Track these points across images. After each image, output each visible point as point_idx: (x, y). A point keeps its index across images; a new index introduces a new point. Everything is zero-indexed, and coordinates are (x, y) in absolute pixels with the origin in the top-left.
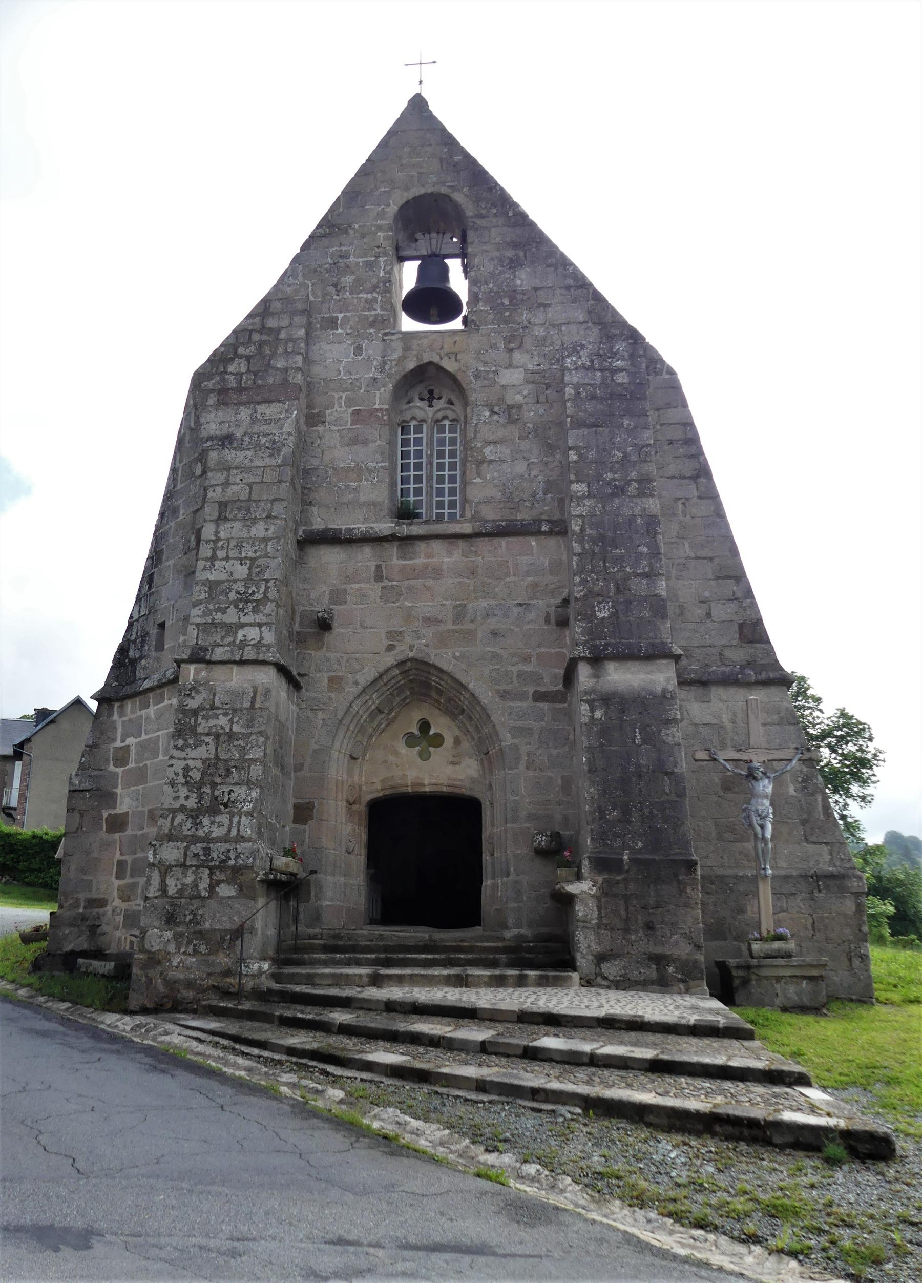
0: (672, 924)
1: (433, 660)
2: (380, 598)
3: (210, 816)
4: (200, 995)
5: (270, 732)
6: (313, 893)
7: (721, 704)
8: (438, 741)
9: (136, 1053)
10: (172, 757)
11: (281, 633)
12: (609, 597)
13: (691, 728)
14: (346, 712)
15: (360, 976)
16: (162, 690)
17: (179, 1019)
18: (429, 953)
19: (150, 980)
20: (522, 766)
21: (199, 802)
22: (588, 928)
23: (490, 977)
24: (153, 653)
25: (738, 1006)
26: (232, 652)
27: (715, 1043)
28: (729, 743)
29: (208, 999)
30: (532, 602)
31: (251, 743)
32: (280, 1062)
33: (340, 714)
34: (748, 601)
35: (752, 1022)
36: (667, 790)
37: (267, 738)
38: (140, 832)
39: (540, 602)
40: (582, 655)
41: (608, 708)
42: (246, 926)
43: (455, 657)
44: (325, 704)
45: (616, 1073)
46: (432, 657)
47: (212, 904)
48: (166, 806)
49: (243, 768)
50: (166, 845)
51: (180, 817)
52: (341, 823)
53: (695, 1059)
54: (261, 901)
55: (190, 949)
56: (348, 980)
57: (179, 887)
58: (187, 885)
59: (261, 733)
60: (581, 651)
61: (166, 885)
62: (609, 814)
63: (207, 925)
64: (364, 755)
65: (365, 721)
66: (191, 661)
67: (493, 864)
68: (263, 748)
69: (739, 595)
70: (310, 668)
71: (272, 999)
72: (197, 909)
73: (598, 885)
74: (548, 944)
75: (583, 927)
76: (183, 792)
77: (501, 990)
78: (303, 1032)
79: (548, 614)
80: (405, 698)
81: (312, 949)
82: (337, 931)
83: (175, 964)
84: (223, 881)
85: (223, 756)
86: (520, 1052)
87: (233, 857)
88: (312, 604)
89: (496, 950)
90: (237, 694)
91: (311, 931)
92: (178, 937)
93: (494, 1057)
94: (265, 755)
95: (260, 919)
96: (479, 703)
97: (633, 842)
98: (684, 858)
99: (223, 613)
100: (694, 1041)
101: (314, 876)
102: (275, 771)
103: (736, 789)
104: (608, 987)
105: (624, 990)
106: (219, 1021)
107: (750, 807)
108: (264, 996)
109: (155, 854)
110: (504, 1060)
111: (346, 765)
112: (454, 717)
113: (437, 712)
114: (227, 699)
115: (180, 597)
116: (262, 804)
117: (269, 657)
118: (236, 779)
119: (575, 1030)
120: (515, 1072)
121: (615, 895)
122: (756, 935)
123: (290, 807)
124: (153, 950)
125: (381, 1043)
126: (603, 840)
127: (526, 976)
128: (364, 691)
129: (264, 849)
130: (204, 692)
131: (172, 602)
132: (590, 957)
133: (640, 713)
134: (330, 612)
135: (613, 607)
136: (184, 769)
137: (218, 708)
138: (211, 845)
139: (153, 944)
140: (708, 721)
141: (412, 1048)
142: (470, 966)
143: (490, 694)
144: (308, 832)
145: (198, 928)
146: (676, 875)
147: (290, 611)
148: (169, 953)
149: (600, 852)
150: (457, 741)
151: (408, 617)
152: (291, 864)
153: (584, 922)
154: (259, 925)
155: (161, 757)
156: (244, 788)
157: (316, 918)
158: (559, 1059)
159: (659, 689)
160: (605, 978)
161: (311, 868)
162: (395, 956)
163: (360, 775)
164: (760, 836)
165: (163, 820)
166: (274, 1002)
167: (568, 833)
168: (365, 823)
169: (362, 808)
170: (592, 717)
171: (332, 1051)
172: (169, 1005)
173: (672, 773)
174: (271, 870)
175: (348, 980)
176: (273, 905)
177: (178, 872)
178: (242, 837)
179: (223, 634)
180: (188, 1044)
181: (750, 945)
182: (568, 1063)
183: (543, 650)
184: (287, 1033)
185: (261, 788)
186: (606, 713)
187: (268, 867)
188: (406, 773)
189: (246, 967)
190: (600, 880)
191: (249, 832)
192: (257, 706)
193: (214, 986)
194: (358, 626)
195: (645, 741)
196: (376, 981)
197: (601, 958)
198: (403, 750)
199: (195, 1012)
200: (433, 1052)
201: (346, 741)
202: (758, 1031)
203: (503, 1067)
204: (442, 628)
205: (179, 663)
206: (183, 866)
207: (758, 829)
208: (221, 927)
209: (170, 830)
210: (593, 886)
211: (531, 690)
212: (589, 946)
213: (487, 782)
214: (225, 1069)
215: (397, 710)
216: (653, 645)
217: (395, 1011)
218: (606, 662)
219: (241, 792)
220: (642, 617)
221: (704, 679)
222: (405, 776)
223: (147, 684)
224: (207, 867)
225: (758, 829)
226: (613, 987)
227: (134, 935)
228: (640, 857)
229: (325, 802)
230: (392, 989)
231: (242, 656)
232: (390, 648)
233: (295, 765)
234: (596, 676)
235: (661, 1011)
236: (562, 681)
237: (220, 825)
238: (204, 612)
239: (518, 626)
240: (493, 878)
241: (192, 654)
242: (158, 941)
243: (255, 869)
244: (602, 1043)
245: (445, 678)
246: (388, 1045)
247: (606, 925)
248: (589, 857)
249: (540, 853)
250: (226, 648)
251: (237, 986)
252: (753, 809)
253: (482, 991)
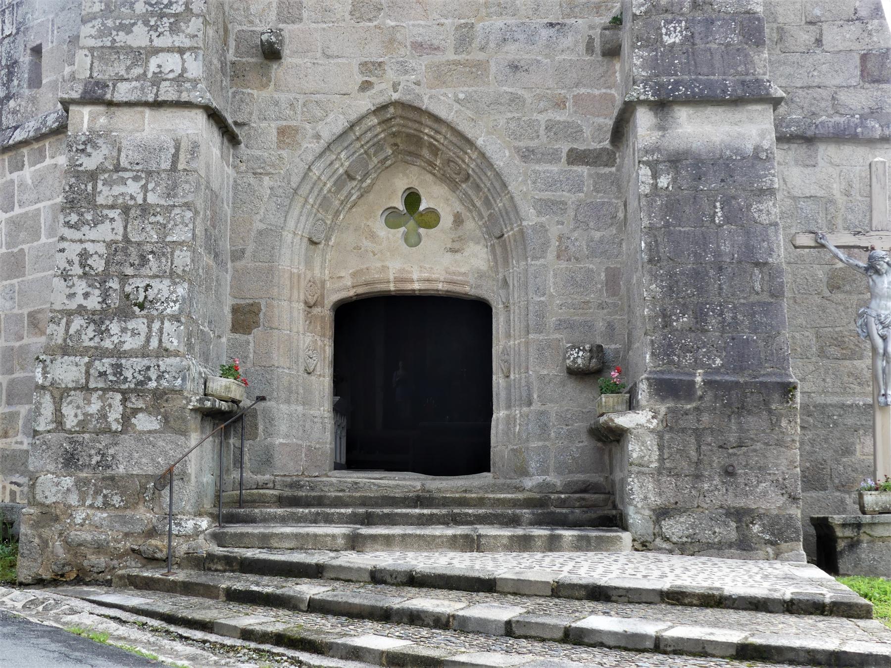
0: (760, 468)
1: (426, 104)
2: (351, 14)
3: (119, 321)
4: (115, 562)
5: (200, 204)
6: (261, 427)
7: (831, 169)
8: (431, 219)
9: (38, 637)
10: (62, 239)
11: (211, 63)
12: (682, 15)
13: (789, 202)
14: (304, 178)
15: (334, 537)
16: (41, 144)
17: (88, 593)
18: (422, 506)
19: (45, 543)
20: (551, 255)
21: (104, 301)
22: (644, 474)
23: (511, 538)
24: (26, 92)
25: (844, 575)
26: (142, 89)
27: (822, 623)
28: (839, 222)
29: (127, 567)
30: (567, 21)
31: (174, 220)
32: (232, 648)
33: (295, 180)
34: (876, 22)
35: (866, 596)
36: (758, 287)
37: (196, 213)
38: (17, 344)
39: (580, 21)
40: (642, 97)
41: (677, 172)
42: (176, 471)
43: (458, 101)
44: (273, 166)
45: (691, 662)
46: (426, 101)
47: (127, 440)
48: (57, 307)
49: (164, 254)
50: (59, 360)
51: (78, 323)
52: (298, 332)
53: (796, 643)
54: (194, 438)
55: (99, 502)
56: (317, 542)
57: (81, 417)
58: (91, 415)
59: (187, 206)
60: (639, 92)
61: (62, 415)
62: (677, 321)
63: (121, 470)
64: (328, 239)
65: (329, 191)
66: (85, 101)
67: (508, 388)
68: (191, 226)
69: (863, 13)
70: (251, 114)
71: (214, 567)
72: (107, 447)
73: (660, 417)
74: (586, 496)
75: (639, 472)
76: (81, 287)
77: (526, 555)
78: (260, 609)
79: (591, 40)
80: (386, 159)
81: (262, 501)
82: (295, 479)
83: (79, 521)
84: (140, 410)
85: (134, 237)
86: (560, 634)
87: (154, 377)
88: (251, 22)
89: (515, 503)
90: (150, 150)
91: (260, 478)
92: (81, 484)
93: (524, 642)
94: (194, 236)
95: (193, 461)
96: (491, 165)
97: (709, 359)
98: (779, 380)
99: (127, 33)
100: (792, 620)
101: (262, 404)
102: (207, 260)
103: (848, 288)
104: (671, 552)
105: (692, 555)
106: (144, 596)
107: (869, 311)
108: (203, 563)
109: (45, 373)
110: (538, 646)
111: (303, 251)
112: (453, 185)
113: (429, 178)
114: (138, 157)
115: (63, 9)
116: (191, 305)
117: (195, 96)
118: (155, 270)
119: (631, 606)
120: (556, 660)
121: (683, 430)
122: (870, 482)
123: (227, 310)
124: (48, 502)
125: (369, 624)
126: (669, 355)
127: (560, 537)
128: (328, 148)
129: (196, 368)
130: (104, 146)
131: (51, 17)
132: (647, 512)
133: (722, 181)
134: (278, 33)
135: (687, 28)
136: (80, 255)
137: (125, 170)
138: (123, 361)
139: (47, 493)
140: (813, 193)
141: (412, 630)
142: (480, 523)
143: (507, 154)
144: (252, 345)
145: (109, 472)
146: (766, 403)
147: (221, 32)
148: (70, 506)
149: (662, 372)
150: (458, 220)
151: (391, 42)
152: (234, 387)
153: (640, 465)
154: (192, 469)
155: (43, 239)
156: (167, 282)
157: (266, 460)
158: (612, 643)
159: (749, 148)
160: (667, 540)
161: (258, 393)
162: (378, 511)
163: (323, 268)
164: (881, 351)
165: (55, 327)
166: (216, 570)
167: (613, 346)
168: (330, 332)
169: (326, 313)
170: (655, 186)
171: (304, 635)
172: (73, 575)
173: (766, 264)
174: (205, 395)
175: (317, 542)
176: (208, 444)
177: (78, 397)
178: (166, 350)
179: (129, 63)
180: (104, 625)
181: (861, 496)
182: (626, 649)
183: (582, 91)
184: (239, 612)
185: (190, 283)
186: (674, 180)
187: (201, 391)
188: (387, 263)
189: (177, 524)
190: (663, 409)
191: (176, 343)
192: (181, 166)
193: (133, 550)
194: (319, 55)
195: (727, 220)
196: (355, 543)
197: (662, 513)
198: (382, 231)
199: (108, 583)
200: (441, 636)
201: (303, 219)
202: (876, 608)
203: (539, 654)
204: (439, 58)
205: (66, 104)
206: (85, 388)
207: (879, 342)
208: (140, 472)
209: (65, 340)
210: (653, 417)
211: (565, 147)
212: (646, 498)
213: (500, 276)
214: (161, 658)
215: (374, 175)
216: (743, 83)
217: (384, 582)
218: (676, 108)
219: (162, 288)
220: (728, 45)
221: (809, 133)
222: (385, 268)
223: (19, 136)
224: (118, 391)
225: (879, 342)
226: (677, 551)
227: (15, 483)
228: (718, 378)
229: (275, 303)
230: (378, 553)
231: (157, 95)
232: (366, 86)
233: (232, 252)
234: (662, 128)
235: (745, 582)
236: (609, 135)
237: (135, 333)
238: (99, 30)
239: (547, 56)
240: (509, 407)
241: (85, 92)
242: (54, 489)
243: (185, 394)
244: (670, 624)
245: (444, 130)
246: (378, 626)
247: (670, 470)
248: (648, 379)
249: (577, 374)
250: (134, 83)
251: (165, 551)
252: (874, 314)
253: (500, 556)
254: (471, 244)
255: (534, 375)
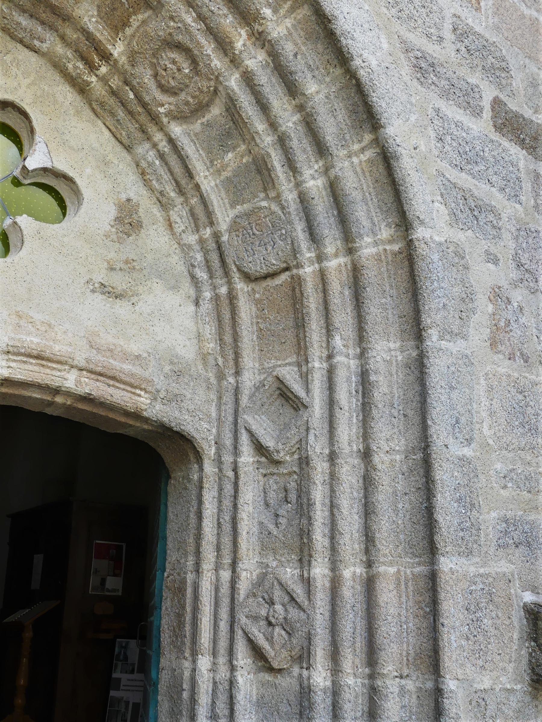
254: (158, 287)
255: (460, 694)
